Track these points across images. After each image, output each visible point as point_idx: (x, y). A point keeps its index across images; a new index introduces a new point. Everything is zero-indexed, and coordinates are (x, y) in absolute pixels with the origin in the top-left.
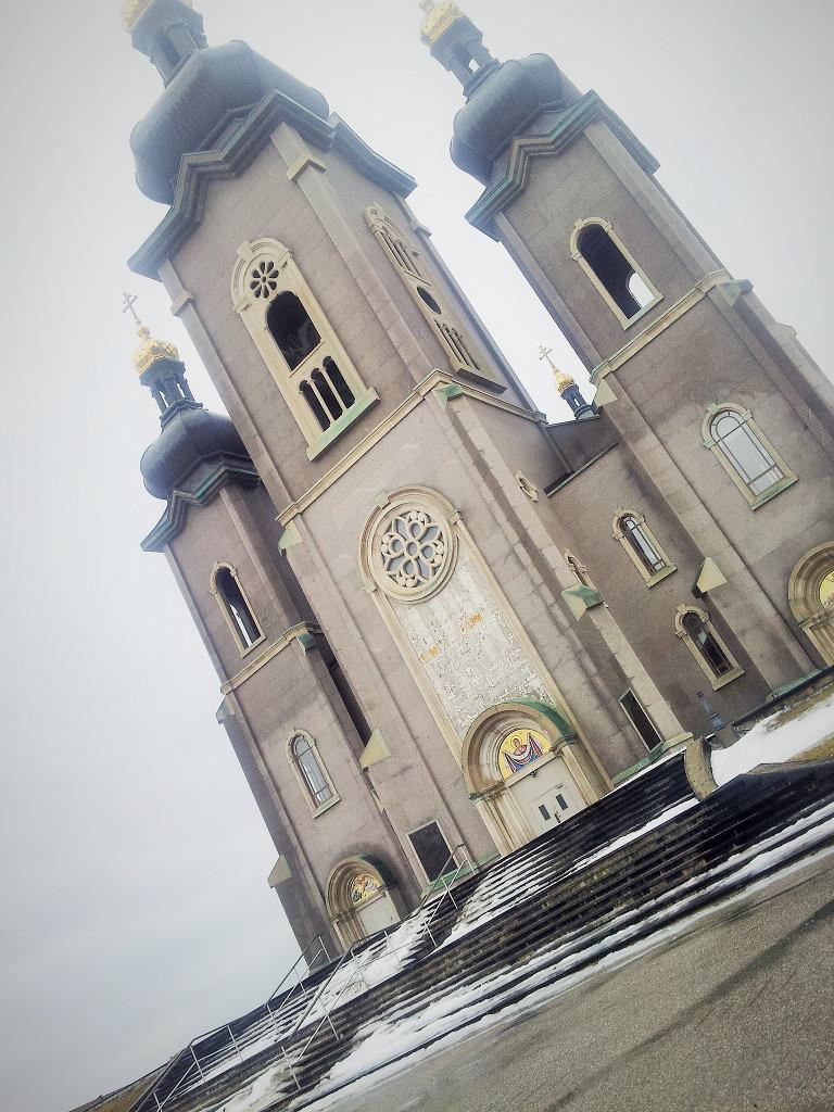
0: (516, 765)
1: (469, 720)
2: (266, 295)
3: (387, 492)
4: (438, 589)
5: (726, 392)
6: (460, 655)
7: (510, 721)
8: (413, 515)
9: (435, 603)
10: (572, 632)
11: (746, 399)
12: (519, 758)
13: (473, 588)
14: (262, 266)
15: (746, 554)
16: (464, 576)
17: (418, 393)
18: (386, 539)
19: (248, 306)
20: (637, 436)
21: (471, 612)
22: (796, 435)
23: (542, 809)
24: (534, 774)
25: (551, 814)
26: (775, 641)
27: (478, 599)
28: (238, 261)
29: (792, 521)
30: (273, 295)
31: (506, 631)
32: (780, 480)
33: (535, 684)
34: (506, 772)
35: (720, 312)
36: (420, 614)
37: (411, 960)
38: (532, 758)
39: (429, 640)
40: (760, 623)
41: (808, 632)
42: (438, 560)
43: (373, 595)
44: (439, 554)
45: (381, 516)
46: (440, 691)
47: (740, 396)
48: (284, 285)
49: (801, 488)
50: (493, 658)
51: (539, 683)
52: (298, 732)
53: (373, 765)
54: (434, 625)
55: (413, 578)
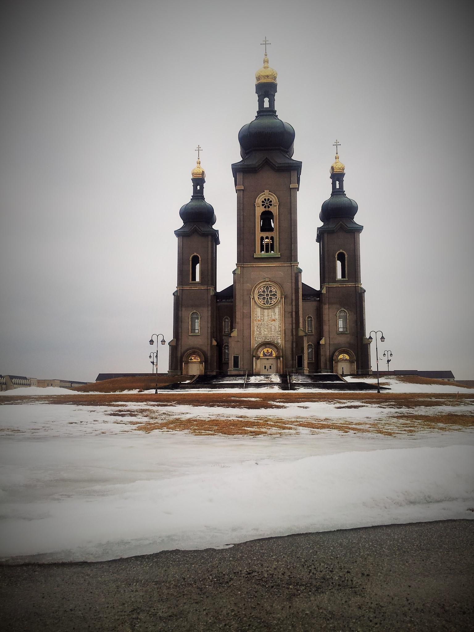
0: (264, 355)
1: (260, 340)
2: (265, 207)
3: (269, 279)
4: (268, 308)
5: (347, 308)
6: (265, 325)
7: (270, 346)
8: (272, 288)
9: (266, 311)
10: (295, 337)
11: (350, 312)
12: (267, 354)
13: (277, 313)
14: (268, 199)
15: (331, 341)
16: (277, 310)
17: (291, 264)
18: (262, 289)
19: (259, 206)
20: (325, 304)
21: (273, 318)
22: (354, 325)
23: (265, 367)
24: (268, 359)
25: (267, 368)
26: (326, 360)
27: (277, 317)
28: (263, 193)
29: (342, 340)
30: (267, 209)
31: (280, 327)
32: (345, 331)
33: (279, 341)
34: (261, 355)
35: (356, 292)
36: (261, 311)
37: (296, 387)
38: (270, 355)
39: (259, 317)
40: (325, 355)
41: (334, 362)
42: (273, 302)
43: (252, 299)
44: (274, 301)
45: (265, 283)
46: (256, 330)
47: (349, 311)
48: (270, 209)
49: (349, 335)
50: (273, 331)
51: (280, 341)
52: (197, 312)
53: (233, 336)
54: (263, 315)
55: (264, 302)
